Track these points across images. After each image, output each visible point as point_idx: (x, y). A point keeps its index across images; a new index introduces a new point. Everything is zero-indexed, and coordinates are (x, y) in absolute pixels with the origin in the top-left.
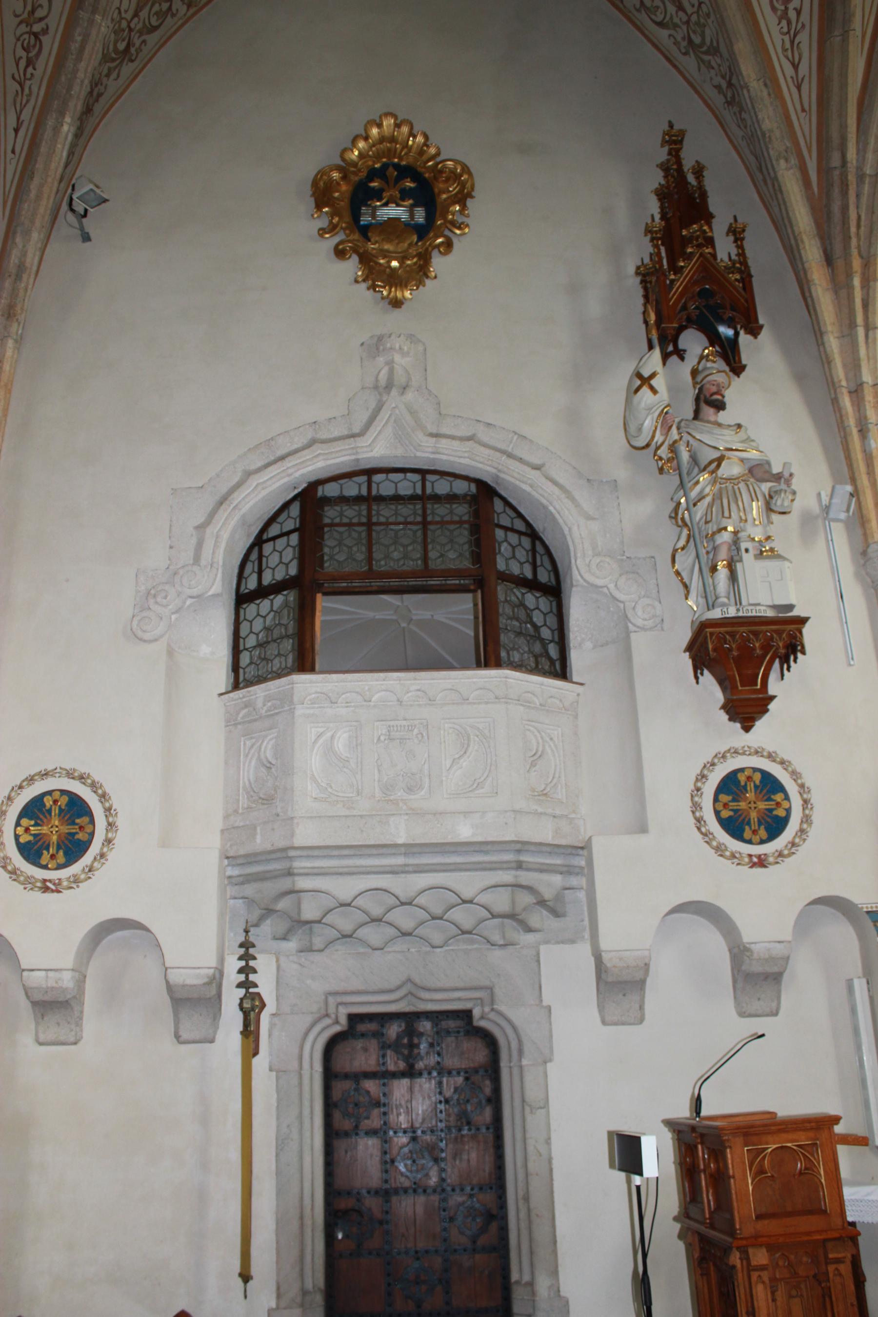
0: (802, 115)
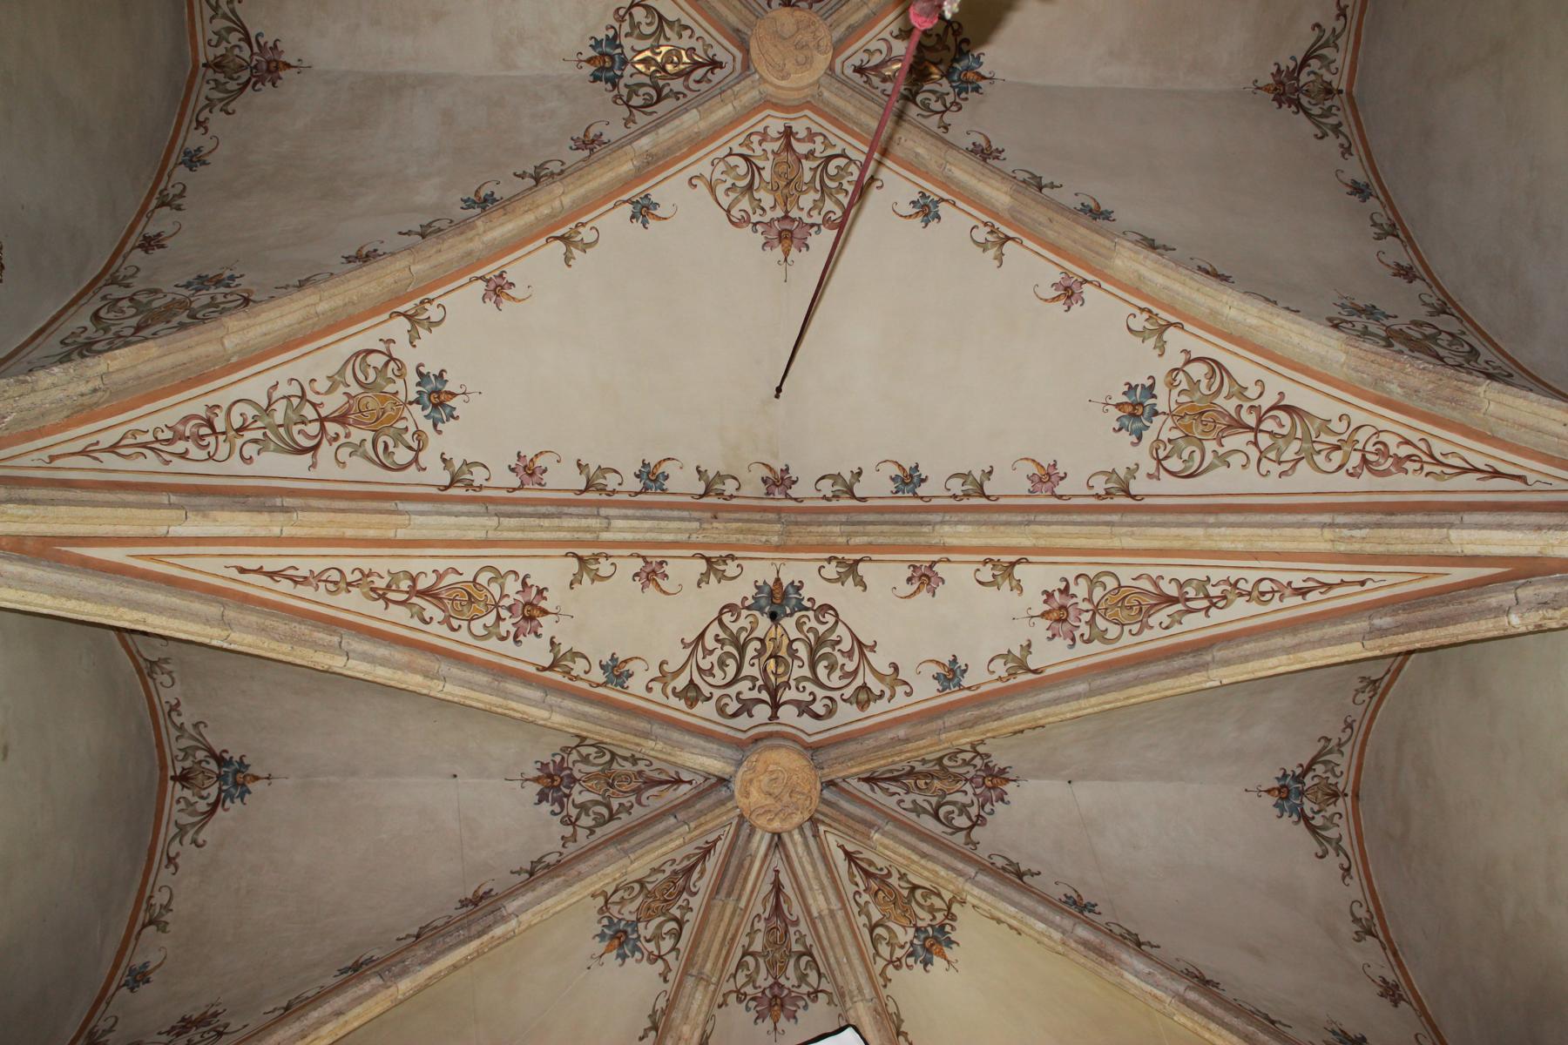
0: (45, 455)
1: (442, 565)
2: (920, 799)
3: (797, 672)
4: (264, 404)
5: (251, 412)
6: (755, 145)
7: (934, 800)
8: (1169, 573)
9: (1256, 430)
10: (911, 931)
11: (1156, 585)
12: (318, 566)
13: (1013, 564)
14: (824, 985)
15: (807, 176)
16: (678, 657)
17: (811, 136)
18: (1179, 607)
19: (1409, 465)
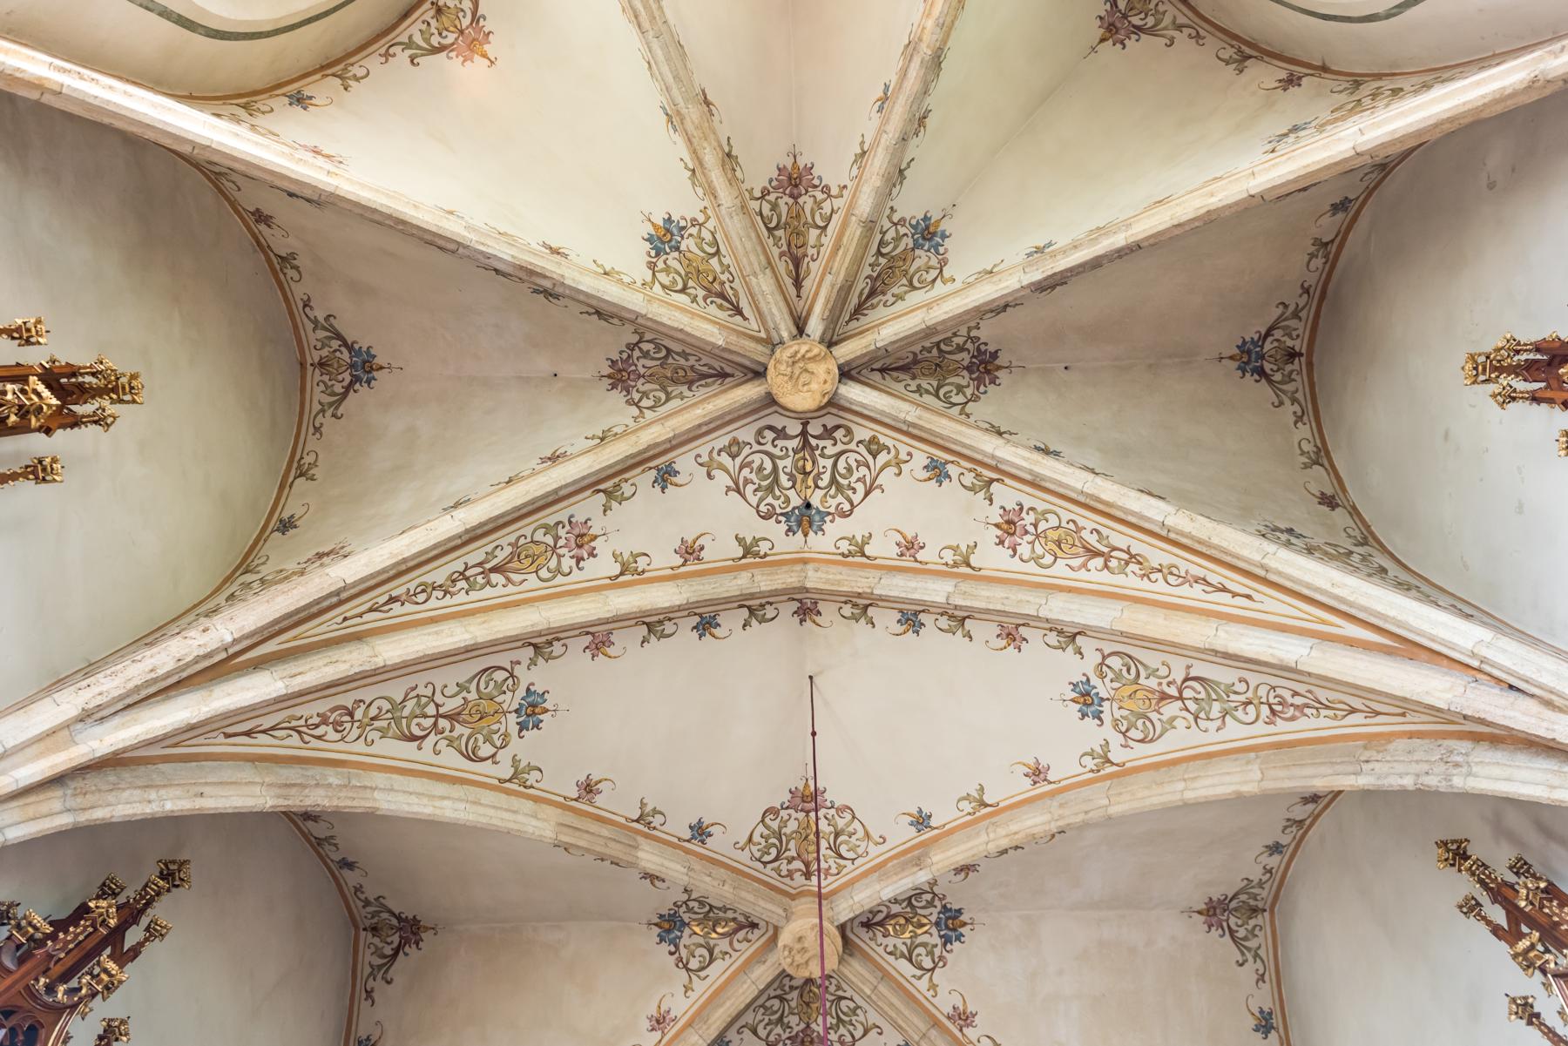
0: (1409, 718)
1: (1082, 574)
2: (682, 361)
3: (788, 462)
4: (1228, 718)
5: (1240, 714)
6: (834, 866)
7: (670, 361)
8: (499, 591)
9: (438, 716)
10: (683, 247)
11: (508, 579)
12: (1185, 590)
13: (622, 574)
14: (755, 205)
15: (792, 845)
16: (886, 478)
17: (790, 874)
18: (488, 566)
19: (316, 720)
